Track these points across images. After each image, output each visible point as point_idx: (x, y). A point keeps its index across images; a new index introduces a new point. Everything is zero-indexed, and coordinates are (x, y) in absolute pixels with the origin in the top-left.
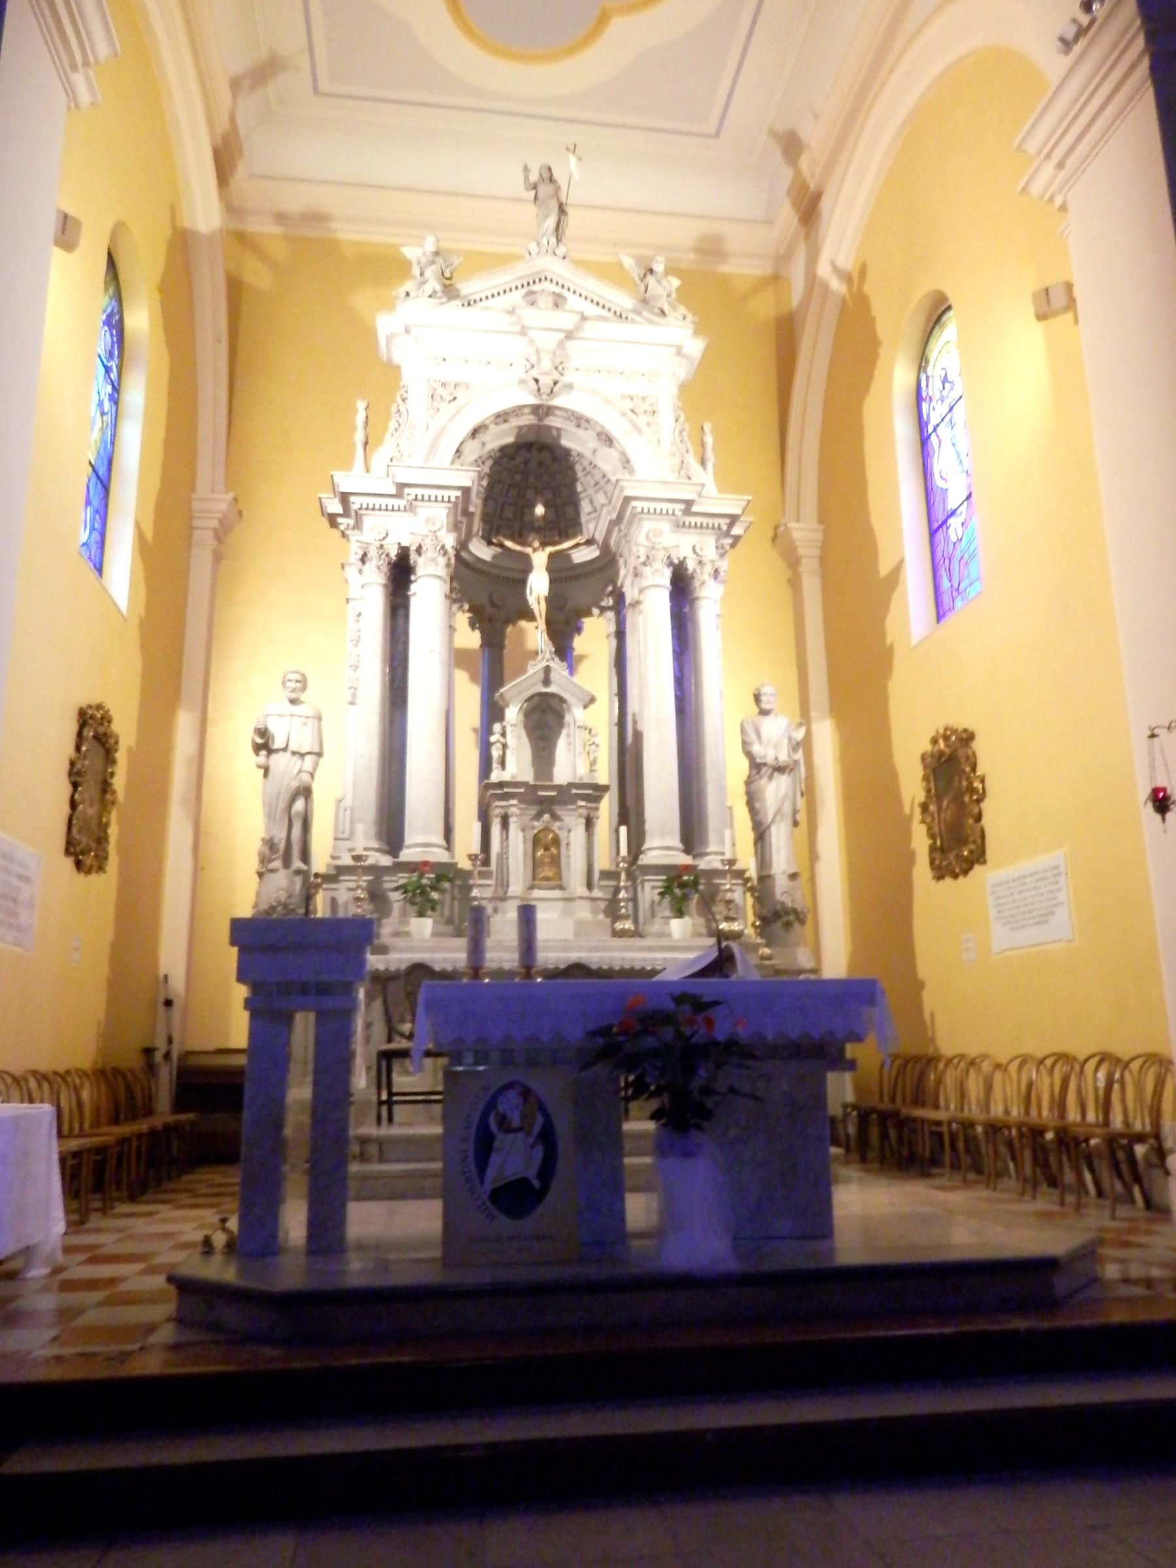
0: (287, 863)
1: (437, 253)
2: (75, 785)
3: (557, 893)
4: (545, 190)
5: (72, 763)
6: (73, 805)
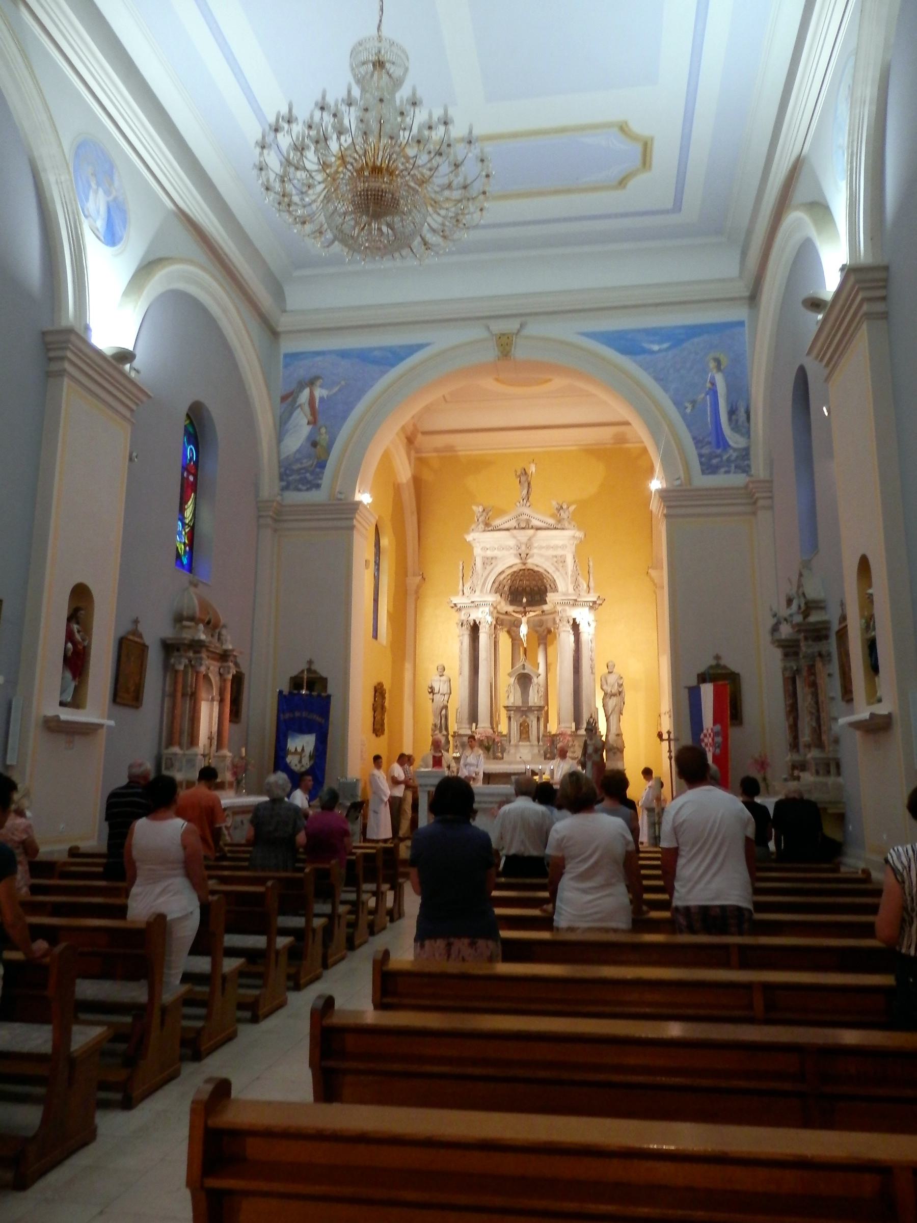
0: (441, 731)
1: (484, 510)
2: (375, 712)
3: (528, 743)
4: (523, 479)
5: (373, 705)
6: (374, 718)
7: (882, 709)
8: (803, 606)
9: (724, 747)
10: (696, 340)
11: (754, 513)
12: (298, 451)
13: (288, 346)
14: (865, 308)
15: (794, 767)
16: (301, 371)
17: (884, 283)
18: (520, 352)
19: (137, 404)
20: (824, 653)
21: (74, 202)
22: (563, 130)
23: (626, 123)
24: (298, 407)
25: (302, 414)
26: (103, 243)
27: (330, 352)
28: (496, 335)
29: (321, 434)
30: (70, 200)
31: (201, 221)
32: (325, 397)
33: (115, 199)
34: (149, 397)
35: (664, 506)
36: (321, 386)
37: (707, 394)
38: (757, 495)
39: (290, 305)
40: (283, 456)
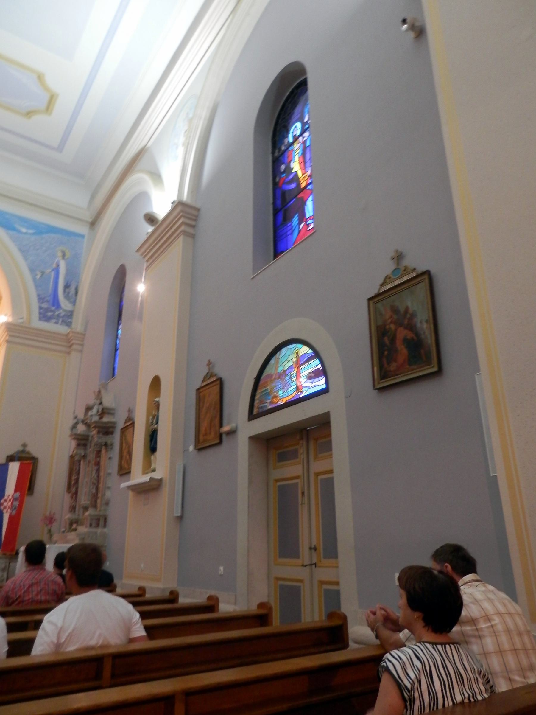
7: (157, 475)
8: (100, 410)
9: (19, 509)
11: (69, 353)
14: (183, 228)
15: (71, 524)
17: (196, 218)
20: (109, 442)
35: (7, 335)
38: (74, 341)
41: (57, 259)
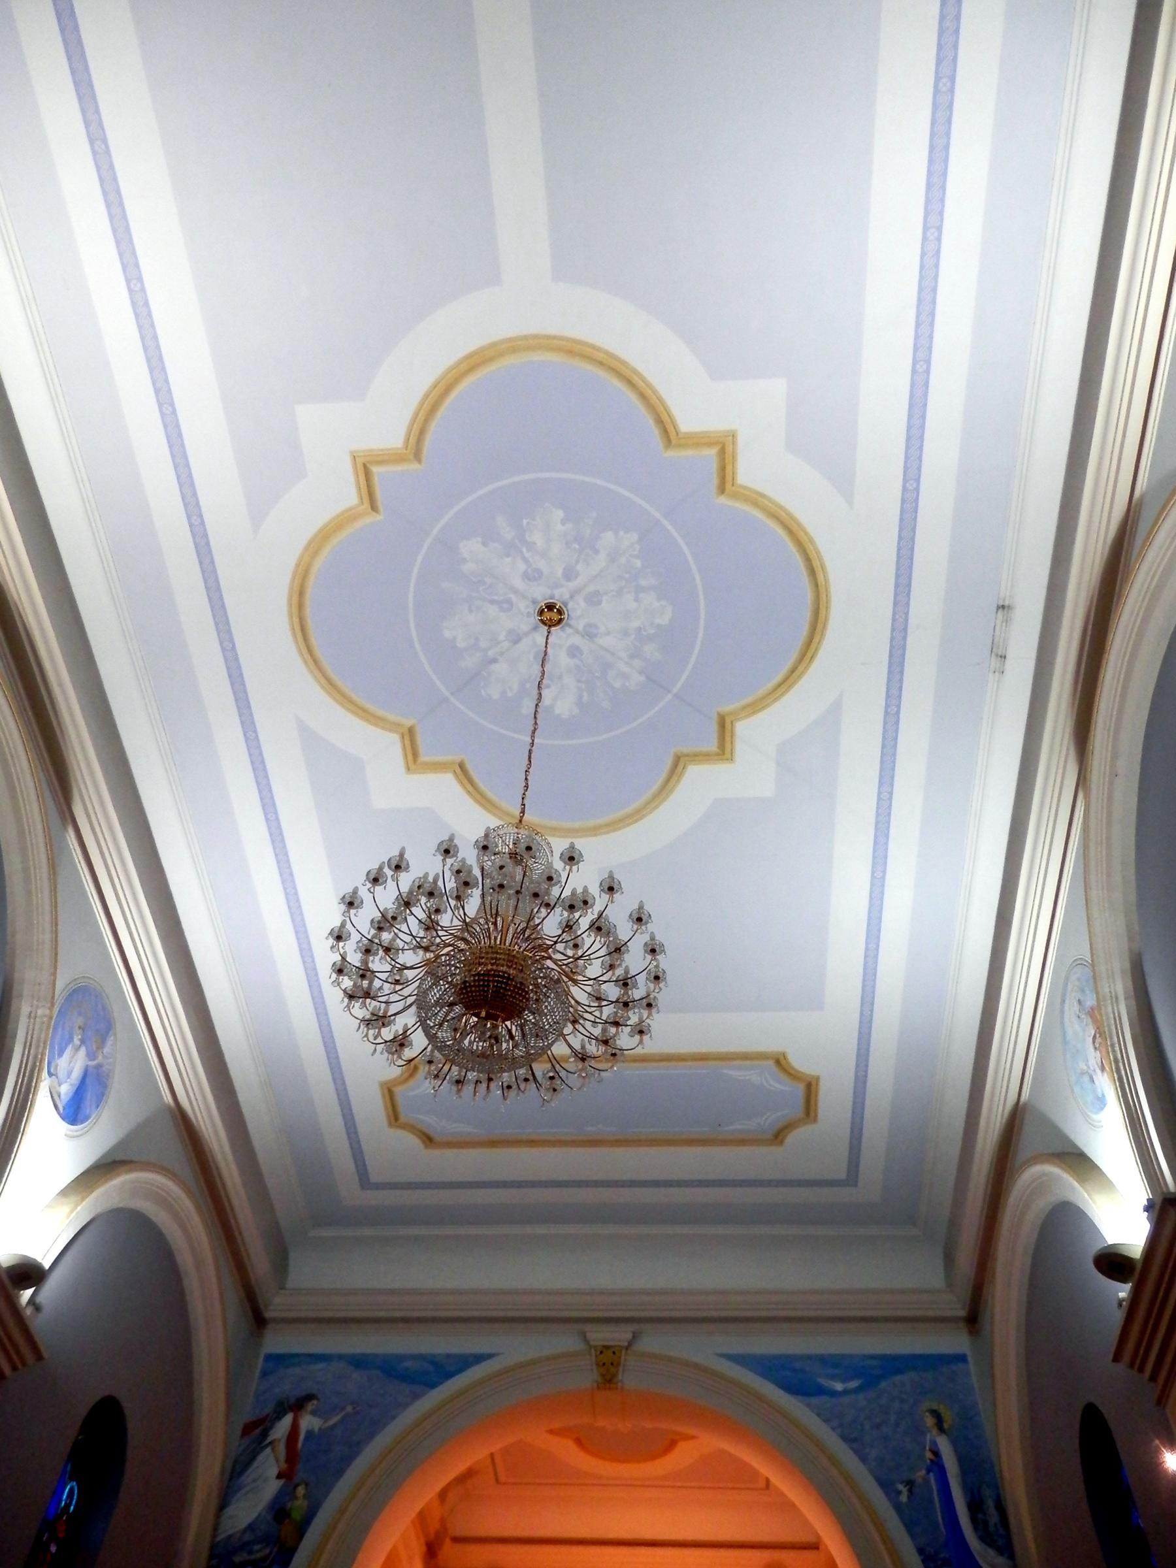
10: (898, 1378)
12: (251, 1527)
13: (276, 1342)
16: (288, 1385)
18: (630, 1379)
19: (15, 1368)
21: (42, 1045)
22: (703, 1058)
23: (784, 1055)
24: (267, 1446)
25: (272, 1460)
26: (59, 1113)
27: (340, 1357)
28: (595, 1347)
29: (296, 1498)
30: (38, 1041)
31: (203, 1128)
32: (316, 1430)
33: (99, 1066)
34: (39, 1357)
36: (314, 1413)
37: (929, 1471)
39: (290, 1283)
40: (221, 1537)
41: (928, 1437)
